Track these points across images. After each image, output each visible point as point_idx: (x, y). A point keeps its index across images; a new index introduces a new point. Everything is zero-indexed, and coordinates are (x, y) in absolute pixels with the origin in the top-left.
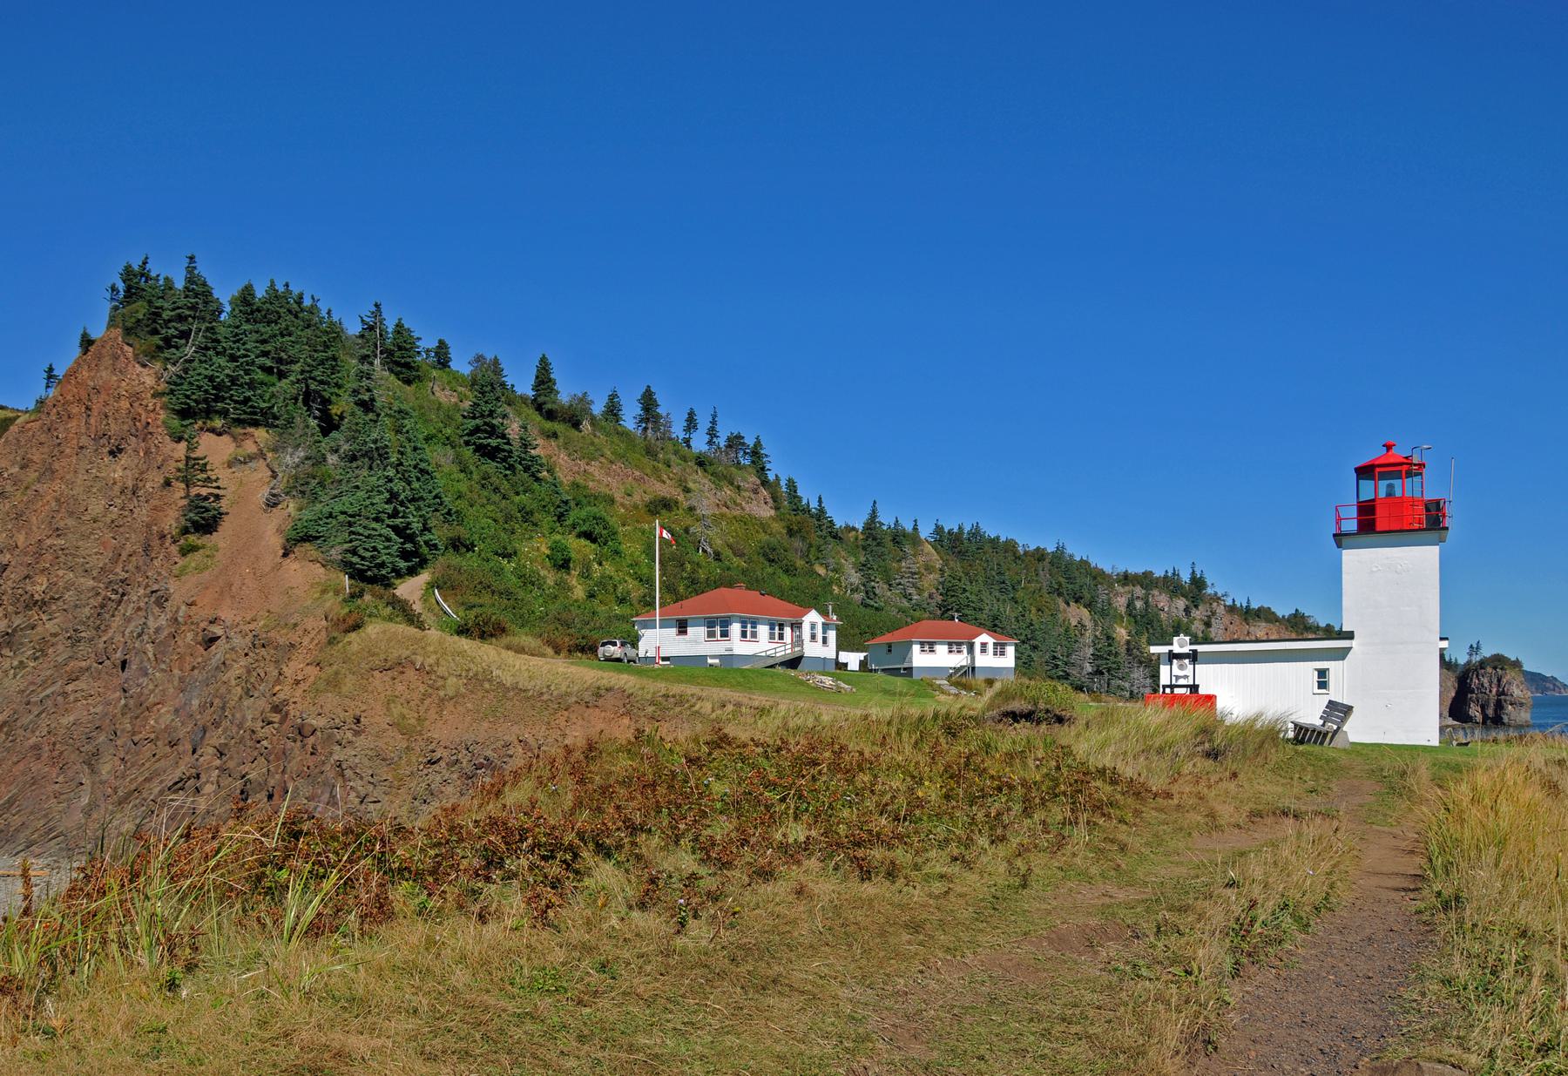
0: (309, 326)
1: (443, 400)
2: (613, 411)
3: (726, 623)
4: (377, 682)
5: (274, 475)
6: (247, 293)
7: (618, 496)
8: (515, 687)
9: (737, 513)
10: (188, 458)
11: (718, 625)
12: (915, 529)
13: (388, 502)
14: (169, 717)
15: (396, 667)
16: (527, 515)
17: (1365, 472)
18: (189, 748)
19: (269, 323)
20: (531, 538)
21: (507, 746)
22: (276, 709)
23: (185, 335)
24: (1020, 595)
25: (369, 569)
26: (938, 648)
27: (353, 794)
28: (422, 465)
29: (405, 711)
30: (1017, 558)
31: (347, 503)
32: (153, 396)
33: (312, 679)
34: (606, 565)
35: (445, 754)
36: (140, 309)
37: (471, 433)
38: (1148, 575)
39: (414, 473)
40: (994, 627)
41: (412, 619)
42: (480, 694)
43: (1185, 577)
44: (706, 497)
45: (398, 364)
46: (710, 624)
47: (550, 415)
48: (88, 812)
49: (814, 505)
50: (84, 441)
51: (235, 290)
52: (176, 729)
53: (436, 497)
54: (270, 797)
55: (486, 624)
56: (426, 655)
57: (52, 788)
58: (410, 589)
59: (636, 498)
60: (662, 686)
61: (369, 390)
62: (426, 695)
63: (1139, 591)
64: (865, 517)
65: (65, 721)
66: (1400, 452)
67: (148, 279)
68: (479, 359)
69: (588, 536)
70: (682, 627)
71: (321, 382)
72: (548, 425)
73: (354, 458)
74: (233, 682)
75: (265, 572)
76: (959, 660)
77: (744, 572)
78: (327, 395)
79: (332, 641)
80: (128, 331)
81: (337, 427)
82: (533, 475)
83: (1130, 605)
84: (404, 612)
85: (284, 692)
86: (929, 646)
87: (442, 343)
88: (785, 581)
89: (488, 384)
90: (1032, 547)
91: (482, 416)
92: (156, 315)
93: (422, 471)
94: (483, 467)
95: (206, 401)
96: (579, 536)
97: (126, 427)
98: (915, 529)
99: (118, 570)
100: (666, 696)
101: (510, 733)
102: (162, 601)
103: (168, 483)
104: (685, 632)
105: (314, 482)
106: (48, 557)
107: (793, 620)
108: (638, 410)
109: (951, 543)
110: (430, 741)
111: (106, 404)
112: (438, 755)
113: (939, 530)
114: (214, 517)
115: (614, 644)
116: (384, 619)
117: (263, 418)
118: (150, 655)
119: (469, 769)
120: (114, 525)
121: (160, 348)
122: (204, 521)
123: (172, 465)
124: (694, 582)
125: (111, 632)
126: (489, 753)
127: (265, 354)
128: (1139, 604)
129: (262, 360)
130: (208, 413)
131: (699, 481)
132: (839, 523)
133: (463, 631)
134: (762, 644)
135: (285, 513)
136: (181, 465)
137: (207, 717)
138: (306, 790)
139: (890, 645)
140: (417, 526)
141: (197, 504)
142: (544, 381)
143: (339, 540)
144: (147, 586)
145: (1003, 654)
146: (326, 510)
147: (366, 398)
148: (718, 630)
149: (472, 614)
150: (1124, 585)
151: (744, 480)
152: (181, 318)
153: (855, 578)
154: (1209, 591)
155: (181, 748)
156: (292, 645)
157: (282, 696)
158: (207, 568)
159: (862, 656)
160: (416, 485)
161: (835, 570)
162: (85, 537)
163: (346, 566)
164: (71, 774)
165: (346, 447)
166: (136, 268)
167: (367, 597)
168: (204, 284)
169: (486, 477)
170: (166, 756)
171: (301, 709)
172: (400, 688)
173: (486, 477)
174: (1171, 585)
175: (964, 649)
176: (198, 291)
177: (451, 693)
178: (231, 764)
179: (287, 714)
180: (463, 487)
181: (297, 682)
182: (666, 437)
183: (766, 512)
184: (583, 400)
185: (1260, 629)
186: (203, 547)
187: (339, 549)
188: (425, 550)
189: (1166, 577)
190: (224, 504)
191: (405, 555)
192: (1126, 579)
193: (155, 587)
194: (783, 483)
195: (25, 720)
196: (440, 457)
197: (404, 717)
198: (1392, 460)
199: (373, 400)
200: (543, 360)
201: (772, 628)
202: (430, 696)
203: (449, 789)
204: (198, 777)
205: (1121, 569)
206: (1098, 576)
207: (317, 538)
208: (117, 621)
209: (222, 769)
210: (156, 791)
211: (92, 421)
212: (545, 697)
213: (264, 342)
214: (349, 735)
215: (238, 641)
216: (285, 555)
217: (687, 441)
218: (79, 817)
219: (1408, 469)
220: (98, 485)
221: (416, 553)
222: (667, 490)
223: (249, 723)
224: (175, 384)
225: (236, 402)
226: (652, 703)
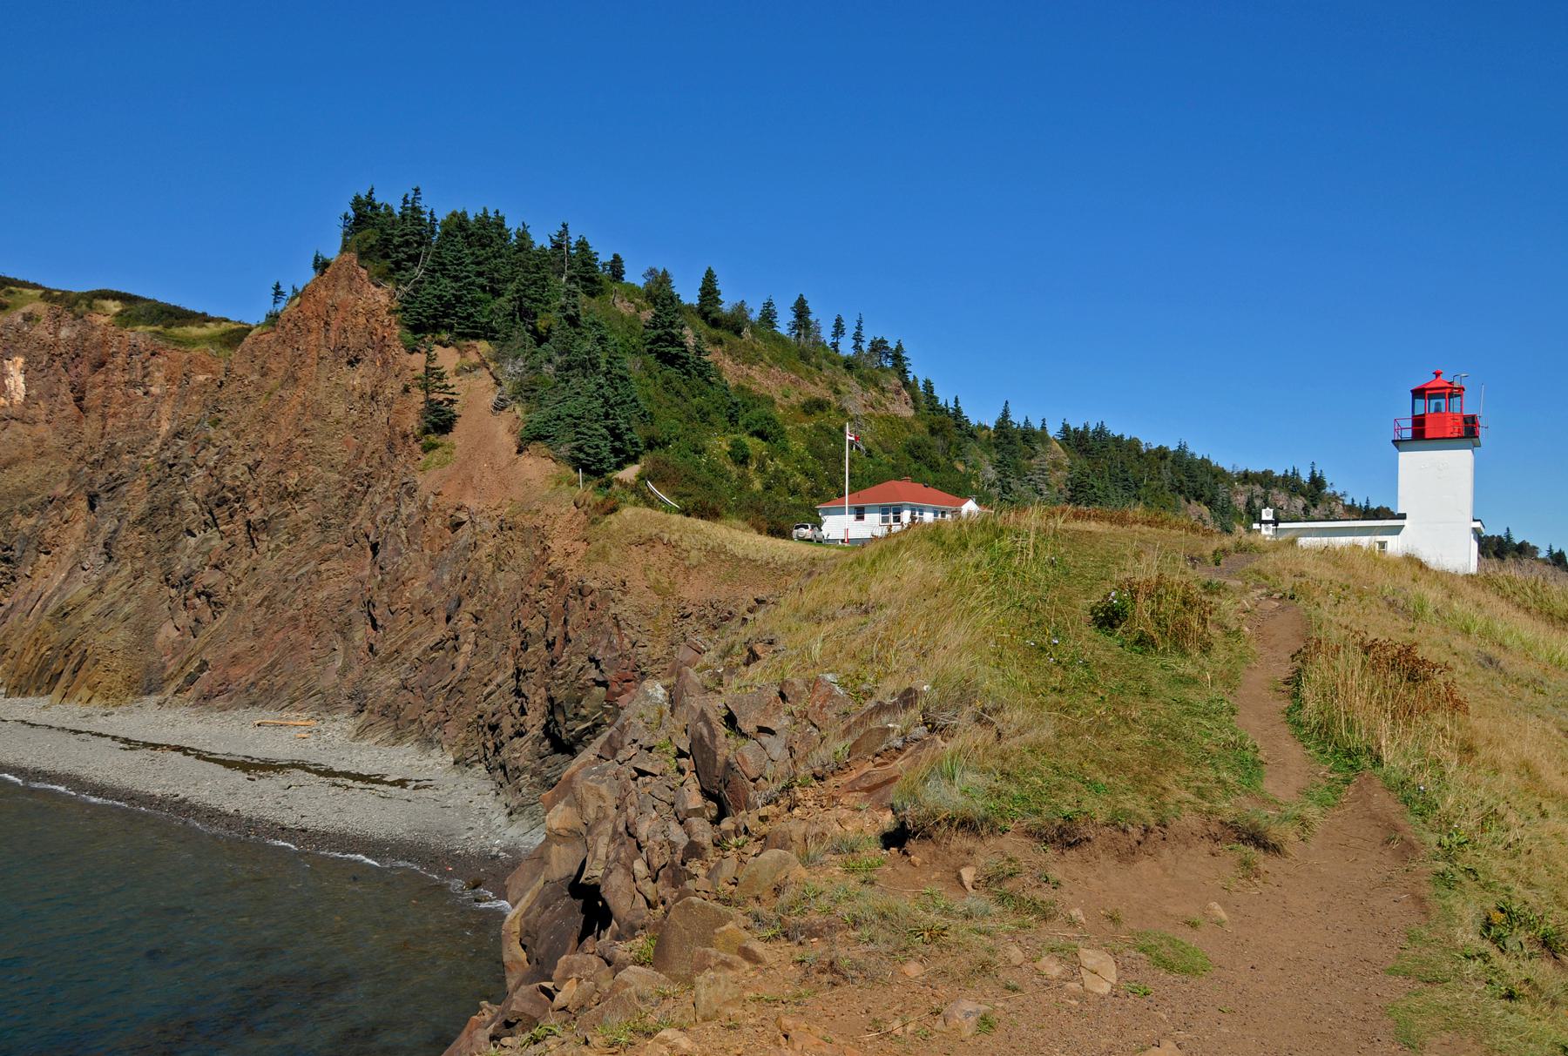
1: (624, 311)
2: (768, 317)
7: (777, 397)
8: (746, 558)
12: (1043, 428)
14: (423, 590)
15: (650, 542)
16: (704, 416)
17: (1418, 393)
18: (443, 615)
19: (484, 246)
22: (551, 576)
23: (414, 259)
24: (1143, 491)
30: (1140, 456)
33: (582, 552)
37: (654, 342)
38: (1267, 474)
42: (718, 563)
43: (1305, 477)
44: (856, 399)
46: (885, 511)
47: (715, 323)
48: (343, 673)
49: (951, 404)
50: (324, 352)
52: (430, 600)
56: (671, 533)
57: (308, 653)
59: (793, 399)
62: (674, 565)
63: (1258, 490)
64: (998, 415)
65: (319, 596)
66: (1446, 377)
67: (374, 208)
68: (652, 272)
69: (760, 434)
70: (860, 514)
71: (534, 300)
72: (714, 332)
73: (569, 367)
75: (497, 463)
77: (894, 467)
80: (363, 256)
81: (546, 339)
85: (557, 562)
87: (616, 257)
88: (930, 476)
89: (659, 293)
90: (1155, 446)
91: (663, 327)
92: (387, 241)
95: (434, 317)
96: (752, 435)
98: (1043, 428)
99: (363, 465)
103: (406, 390)
106: (298, 454)
108: (792, 318)
109: (1076, 441)
110: (681, 600)
111: (344, 320)
112: (688, 610)
113: (1066, 428)
117: (488, 333)
119: (715, 621)
120: (354, 426)
121: (391, 270)
122: (440, 422)
125: (358, 520)
127: (480, 274)
129: (481, 280)
130: (436, 329)
131: (849, 383)
132: (974, 422)
137: (459, 588)
138: (587, 638)
141: (433, 407)
142: (709, 291)
148: (891, 516)
150: (1244, 483)
151: (888, 382)
152: (407, 244)
153: (992, 474)
154: (1329, 490)
157: (556, 565)
161: (973, 467)
162: (330, 437)
163: (577, 464)
164: (325, 641)
170: (421, 623)
172: (653, 559)
173: (668, 382)
178: (487, 627)
180: (651, 392)
182: (818, 343)
183: (908, 413)
184: (741, 307)
187: (567, 446)
189: (1285, 476)
192: (1246, 478)
194: (921, 384)
195: (284, 595)
204: (457, 638)
205: (1241, 468)
206: (1219, 475)
208: (364, 509)
211: (332, 334)
215: (487, 525)
216: (519, 452)
217: (835, 346)
218: (333, 677)
220: (339, 391)
222: (819, 391)
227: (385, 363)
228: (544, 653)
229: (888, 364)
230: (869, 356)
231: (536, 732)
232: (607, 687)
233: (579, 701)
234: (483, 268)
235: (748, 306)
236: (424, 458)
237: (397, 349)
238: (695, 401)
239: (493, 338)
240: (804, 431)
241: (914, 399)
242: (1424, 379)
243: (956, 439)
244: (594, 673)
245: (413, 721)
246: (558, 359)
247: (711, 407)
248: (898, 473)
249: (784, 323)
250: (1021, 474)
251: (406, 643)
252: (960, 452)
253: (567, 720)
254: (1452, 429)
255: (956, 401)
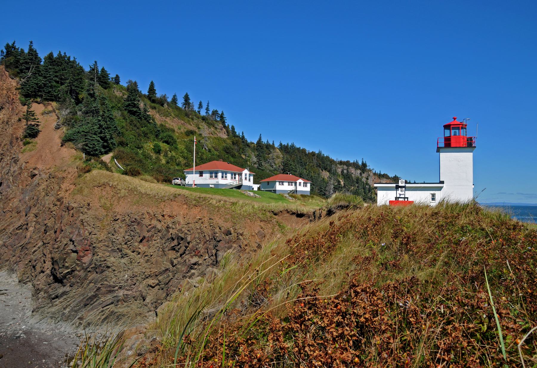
0: (72, 67)
1: (118, 95)
2: (174, 100)
3: (216, 173)
4: (96, 191)
5: (58, 118)
6: (51, 55)
7: (176, 129)
8: (146, 194)
9: (216, 136)
10: (27, 111)
11: (214, 174)
12: (273, 144)
13: (99, 128)
14: (17, 203)
18: (24, 214)
19: (58, 66)
20: (147, 142)
21: (143, 214)
22: (59, 200)
23: (28, 69)
24: (307, 167)
25: (92, 151)
26: (285, 183)
27: (87, 232)
28: (111, 116)
29: (106, 201)
30: (306, 155)
31: (85, 128)
32: (16, 89)
33: (72, 189)
34: (173, 152)
35: (120, 217)
36: (12, 59)
37: (127, 106)
38: (348, 162)
39: (108, 119)
40: (301, 176)
41: (108, 169)
42: (133, 196)
43: (360, 163)
44: (205, 130)
45: (102, 82)
46: (211, 173)
47: (154, 101)
49: (241, 134)
51: (46, 54)
52: (19, 207)
53: (115, 127)
54: (55, 232)
55: (133, 171)
56: (114, 181)
58: (106, 158)
59: (182, 130)
60: (198, 194)
61: (93, 90)
62: (113, 196)
63: (345, 167)
66: (458, 121)
67: (15, 49)
69: (167, 142)
70: (201, 174)
71: (76, 87)
72: (153, 105)
73: (87, 113)
74: (42, 191)
75: (54, 151)
76: (292, 188)
77: (218, 156)
78: (78, 91)
79: (80, 176)
80: (7, 67)
81: (81, 102)
82: (148, 121)
83: (342, 171)
84: (104, 165)
85: (62, 194)
86: (282, 183)
87: (117, 76)
88: (232, 160)
89: (133, 89)
90: (311, 151)
91: (131, 100)
93: (111, 118)
94: (131, 118)
95: (35, 92)
96: (163, 142)
97: (5, 100)
98: (273, 144)
100: (200, 198)
101: (144, 210)
102: (16, 161)
103: (20, 120)
104: (202, 176)
105: (73, 121)
107: (239, 172)
108: (183, 101)
109: (284, 149)
112: (117, 217)
113: (281, 144)
114: (36, 132)
115: (178, 179)
116: (98, 169)
117: (56, 99)
118: (11, 180)
119: (129, 223)
122: (33, 133)
123: (21, 114)
124: (202, 159)
126: (136, 217)
127: (56, 76)
128: (345, 171)
130: (35, 96)
131: (203, 125)
132: (249, 141)
133: (125, 173)
134: (229, 181)
135: (62, 131)
136: (25, 114)
137: (32, 203)
138: (69, 230)
139: (268, 182)
140: (108, 137)
141: (30, 127)
142: (152, 90)
143: (81, 141)
144: (11, 156)
145: (306, 186)
146: (77, 130)
147: (92, 92)
148: (214, 175)
149: (129, 167)
150: (340, 165)
151: (218, 125)
152: (27, 63)
153: (255, 159)
155: (21, 214)
156: (64, 178)
157: (61, 195)
158: (33, 150)
159: (258, 186)
160: (108, 123)
161: (248, 157)
163: (84, 150)
165: (84, 109)
166: (11, 45)
167: (93, 161)
168: (36, 51)
169: (132, 121)
170: (15, 217)
171: (68, 200)
172: (104, 193)
173: (132, 121)
174: (355, 165)
175: (293, 184)
176: (33, 53)
177: (123, 195)
178: (40, 220)
179: (63, 202)
180: (124, 124)
181: (67, 191)
183: (225, 137)
185: (385, 180)
186: (32, 142)
187: (81, 144)
188: (111, 145)
189: (354, 163)
190: (40, 128)
191: (104, 147)
192: (341, 163)
193: (14, 156)
196: (117, 114)
197: (105, 204)
198: (456, 123)
199: (94, 93)
200: (152, 83)
201: (232, 175)
202: (115, 196)
203: (122, 230)
204: (27, 224)
205: (339, 160)
206: (332, 161)
207: (74, 140)
209: (37, 222)
210: (11, 229)
212: (157, 197)
213: (56, 72)
214: (86, 210)
215: (44, 176)
216: (62, 146)
217: (199, 112)
219: (462, 126)
221: (107, 146)
222: (192, 128)
223: (47, 205)
224: (24, 85)
225: (46, 92)
226: (195, 200)
227: (13, 109)
228: (53, 235)
229: (218, 119)
230: (212, 116)
231: (48, 272)
232: (77, 253)
233: (65, 260)
234: (58, 74)
235: (167, 96)
236: (24, 148)
237: (18, 104)
238: (142, 129)
239: (58, 101)
240: (185, 142)
241: (228, 132)
242: (450, 121)
243: (241, 146)
244: (71, 247)
245: (7, 261)
246: (84, 109)
247: (148, 131)
248: (219, 158)
249: (180, 103)
250: (265, 160)
251: (8, 225)
252: (244, 151)
253: (60, 268)
254: (463, 143)
255: (243, 133)
